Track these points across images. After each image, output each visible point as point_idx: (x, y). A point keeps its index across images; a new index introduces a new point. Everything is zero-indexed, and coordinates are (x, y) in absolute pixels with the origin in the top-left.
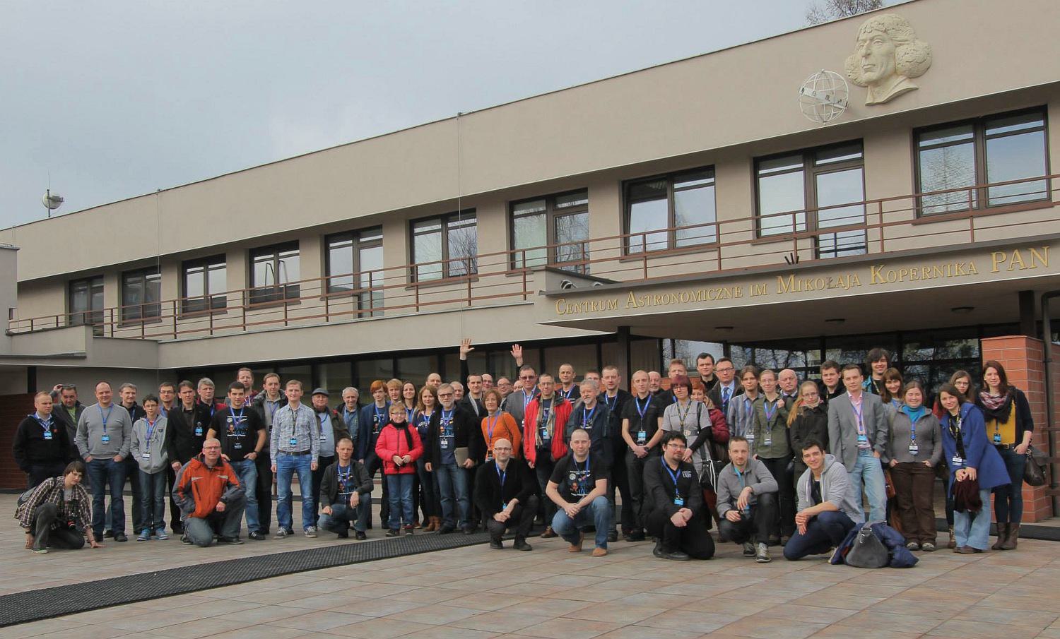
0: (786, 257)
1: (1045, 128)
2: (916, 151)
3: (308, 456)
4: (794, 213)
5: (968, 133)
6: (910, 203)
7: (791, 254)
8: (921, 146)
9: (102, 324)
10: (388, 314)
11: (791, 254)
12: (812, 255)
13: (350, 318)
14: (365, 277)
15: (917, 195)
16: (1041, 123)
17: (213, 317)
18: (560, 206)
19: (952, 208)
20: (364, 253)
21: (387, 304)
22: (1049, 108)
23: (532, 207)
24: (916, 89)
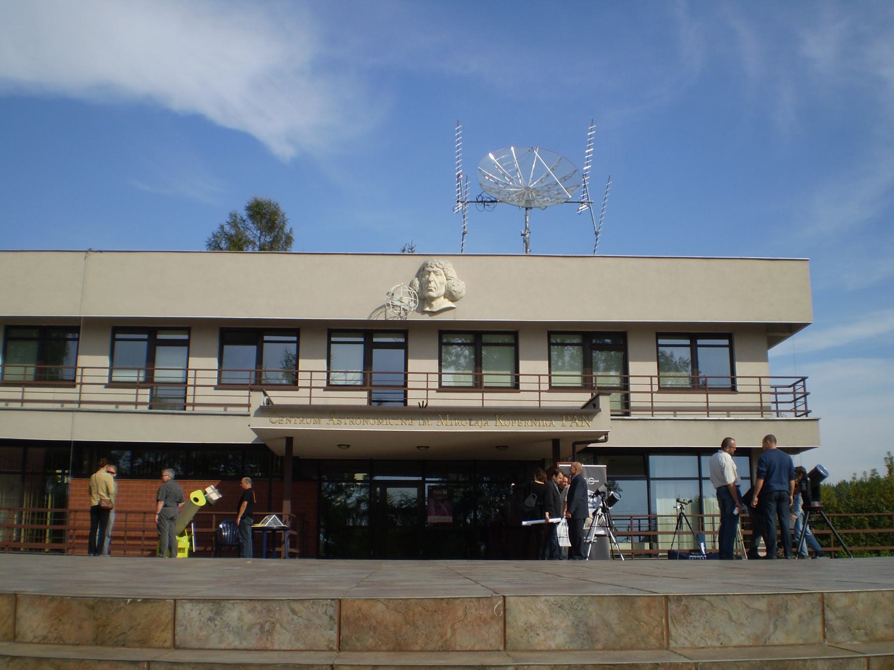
0: (419, 403)
1: (297, 342)
2: (330, 343)
3: (825, 594)
4: (651, 377)
5: (184, 334)
6: (216, 374)
7: (423, 402)
8: (265, 339)
9: (74, 383)
10: (198, 409)
11: (423, 402)
12: (544, 407)
13: (145, 408)
14: (191, 374)
15: (329, 371)
16: (295, 339)
17: (651, 405)
18: (375, 340)
19: (348, 383)
20: (376, 353)
21: (198, 400)
22: (409, 333)
23: (392, 337)
24: (455, 308)
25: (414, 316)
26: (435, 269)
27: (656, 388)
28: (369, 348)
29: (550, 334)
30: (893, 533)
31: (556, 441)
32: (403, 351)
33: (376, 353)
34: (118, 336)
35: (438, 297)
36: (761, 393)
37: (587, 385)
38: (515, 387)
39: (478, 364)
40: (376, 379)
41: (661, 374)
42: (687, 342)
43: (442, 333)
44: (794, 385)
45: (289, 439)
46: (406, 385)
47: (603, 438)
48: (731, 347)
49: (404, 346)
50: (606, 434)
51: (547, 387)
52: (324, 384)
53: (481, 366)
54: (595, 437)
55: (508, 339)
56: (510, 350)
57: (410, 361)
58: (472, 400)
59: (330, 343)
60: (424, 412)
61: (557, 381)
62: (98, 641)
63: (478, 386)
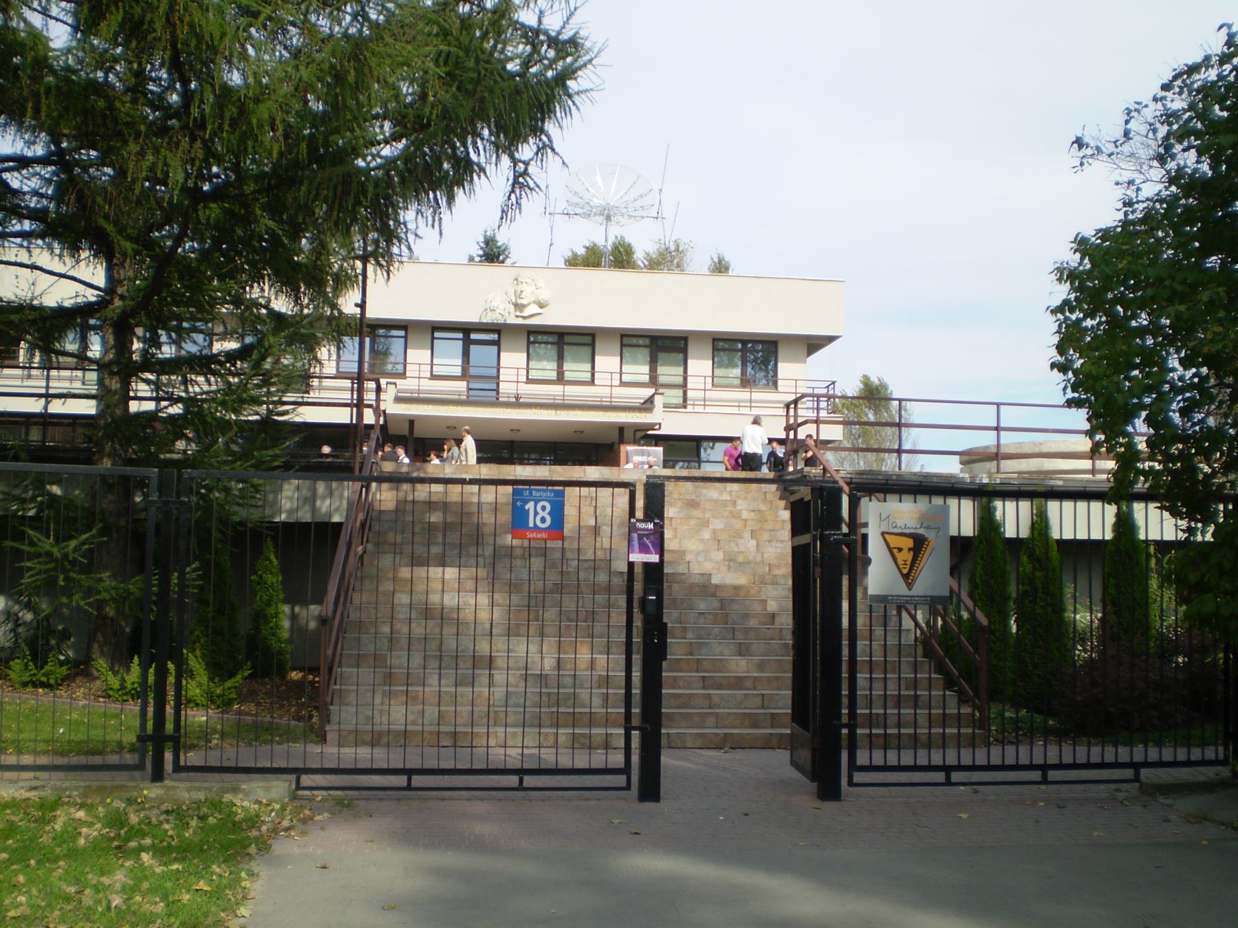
2: (433, 338)
20: (473, 348)
25: (512, 320)
26: (527, 280)
27: (709, 386)
28: (467, 343)
29: (622, 336)
30: (5, 459)
31: (621, 429)
32: (496, 347)
33: (473, 348)
34: (437, 334)
35: (529, 304)
36: (705, 390)
37: (653, 381)
38: (592, 382)
39: (560, 359)
40: (472, 371)
41: (717, 372)
42: (460, 335)
43: (622, 336)
44: (828, 387)
45: (412, 422)
46: (498, 377)
47: (657, 427)
48: (406, 337)
49: (497, 343)
50: (660, 424)
51: (618, 383)
52: (429, 376)
53: (656, 362)
54: (651, 426)
55: (588, 340)
56: (588, 350)
57: (502, 354)
58: (557, 390)
59: (433, 338)
60: (518, 403)
61: (534, 374)
62: (710, 708)
63: (560, 379)
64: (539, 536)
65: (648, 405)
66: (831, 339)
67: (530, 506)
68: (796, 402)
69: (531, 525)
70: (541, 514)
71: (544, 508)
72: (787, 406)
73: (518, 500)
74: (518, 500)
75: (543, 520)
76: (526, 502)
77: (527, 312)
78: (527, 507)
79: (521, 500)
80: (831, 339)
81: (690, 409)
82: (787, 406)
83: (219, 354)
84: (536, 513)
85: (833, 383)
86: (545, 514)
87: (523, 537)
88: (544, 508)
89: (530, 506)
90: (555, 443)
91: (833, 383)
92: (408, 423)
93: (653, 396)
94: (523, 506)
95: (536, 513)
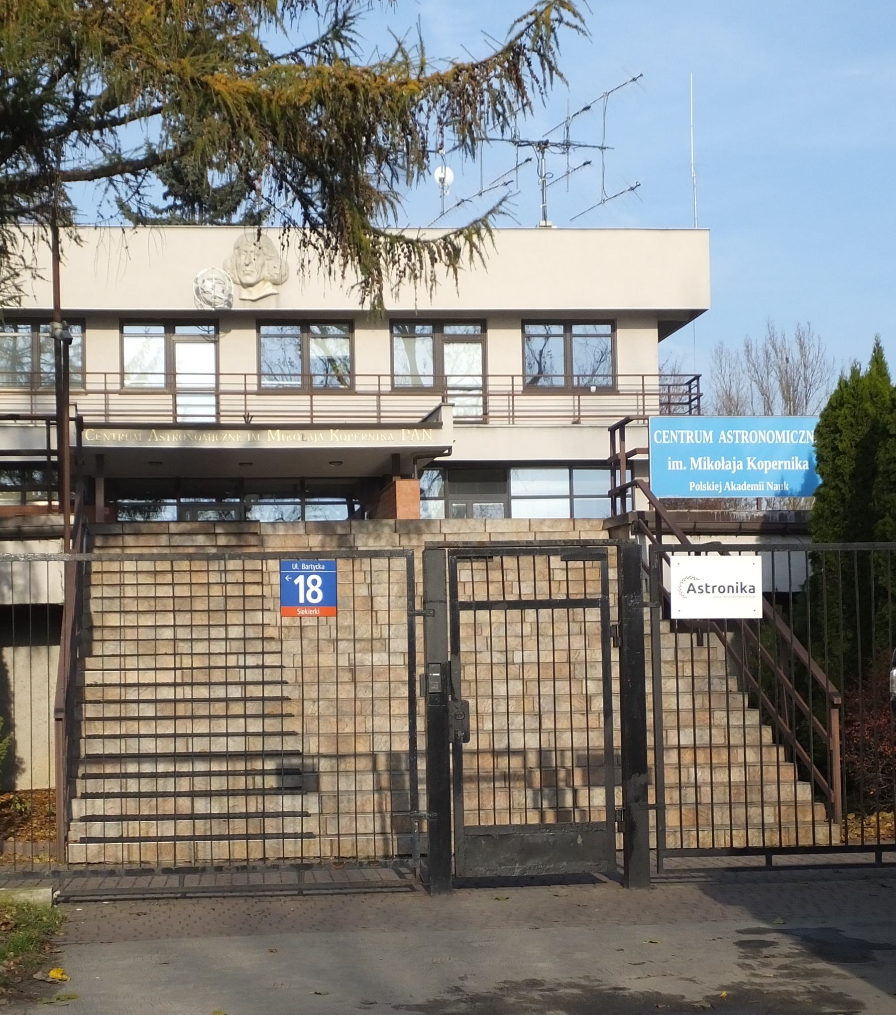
44: (689, 383)
47: (447, 451)
50: (450, 448)
54: (440, 451)
64: (311, 612)
65: (431, 421)
66: (694, 314)
67: (300, 580)
68: (621, 426)
69: (302, 600)
70: (312, 588)
71: (314, 582)
72: (612, 430)
73: (286, 574)
74: (286, 574)
75: (314, 595)
76: (296, 576)
77: (255, 293)
78: (296, 582)
79: (290, 575)
80: (694, 314)
81: (492, 422)
82: (612, 430)
83: (518, 59)
84: (307, 588)
85: (697, 377)
86: (316, 588)
87: (294, 615)
88: (314, 582)
89: (300, 580)
90: (68, 759)
91: (697, 377)
92: (75, 565)
93: (438, 409)
94: (292, 581)
95: (307, 588)
